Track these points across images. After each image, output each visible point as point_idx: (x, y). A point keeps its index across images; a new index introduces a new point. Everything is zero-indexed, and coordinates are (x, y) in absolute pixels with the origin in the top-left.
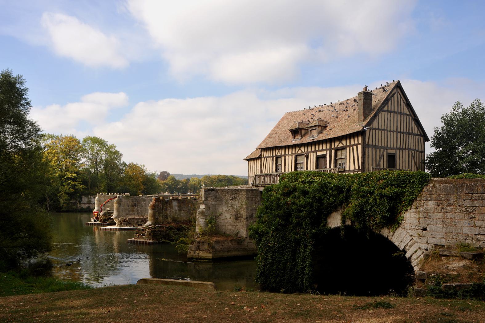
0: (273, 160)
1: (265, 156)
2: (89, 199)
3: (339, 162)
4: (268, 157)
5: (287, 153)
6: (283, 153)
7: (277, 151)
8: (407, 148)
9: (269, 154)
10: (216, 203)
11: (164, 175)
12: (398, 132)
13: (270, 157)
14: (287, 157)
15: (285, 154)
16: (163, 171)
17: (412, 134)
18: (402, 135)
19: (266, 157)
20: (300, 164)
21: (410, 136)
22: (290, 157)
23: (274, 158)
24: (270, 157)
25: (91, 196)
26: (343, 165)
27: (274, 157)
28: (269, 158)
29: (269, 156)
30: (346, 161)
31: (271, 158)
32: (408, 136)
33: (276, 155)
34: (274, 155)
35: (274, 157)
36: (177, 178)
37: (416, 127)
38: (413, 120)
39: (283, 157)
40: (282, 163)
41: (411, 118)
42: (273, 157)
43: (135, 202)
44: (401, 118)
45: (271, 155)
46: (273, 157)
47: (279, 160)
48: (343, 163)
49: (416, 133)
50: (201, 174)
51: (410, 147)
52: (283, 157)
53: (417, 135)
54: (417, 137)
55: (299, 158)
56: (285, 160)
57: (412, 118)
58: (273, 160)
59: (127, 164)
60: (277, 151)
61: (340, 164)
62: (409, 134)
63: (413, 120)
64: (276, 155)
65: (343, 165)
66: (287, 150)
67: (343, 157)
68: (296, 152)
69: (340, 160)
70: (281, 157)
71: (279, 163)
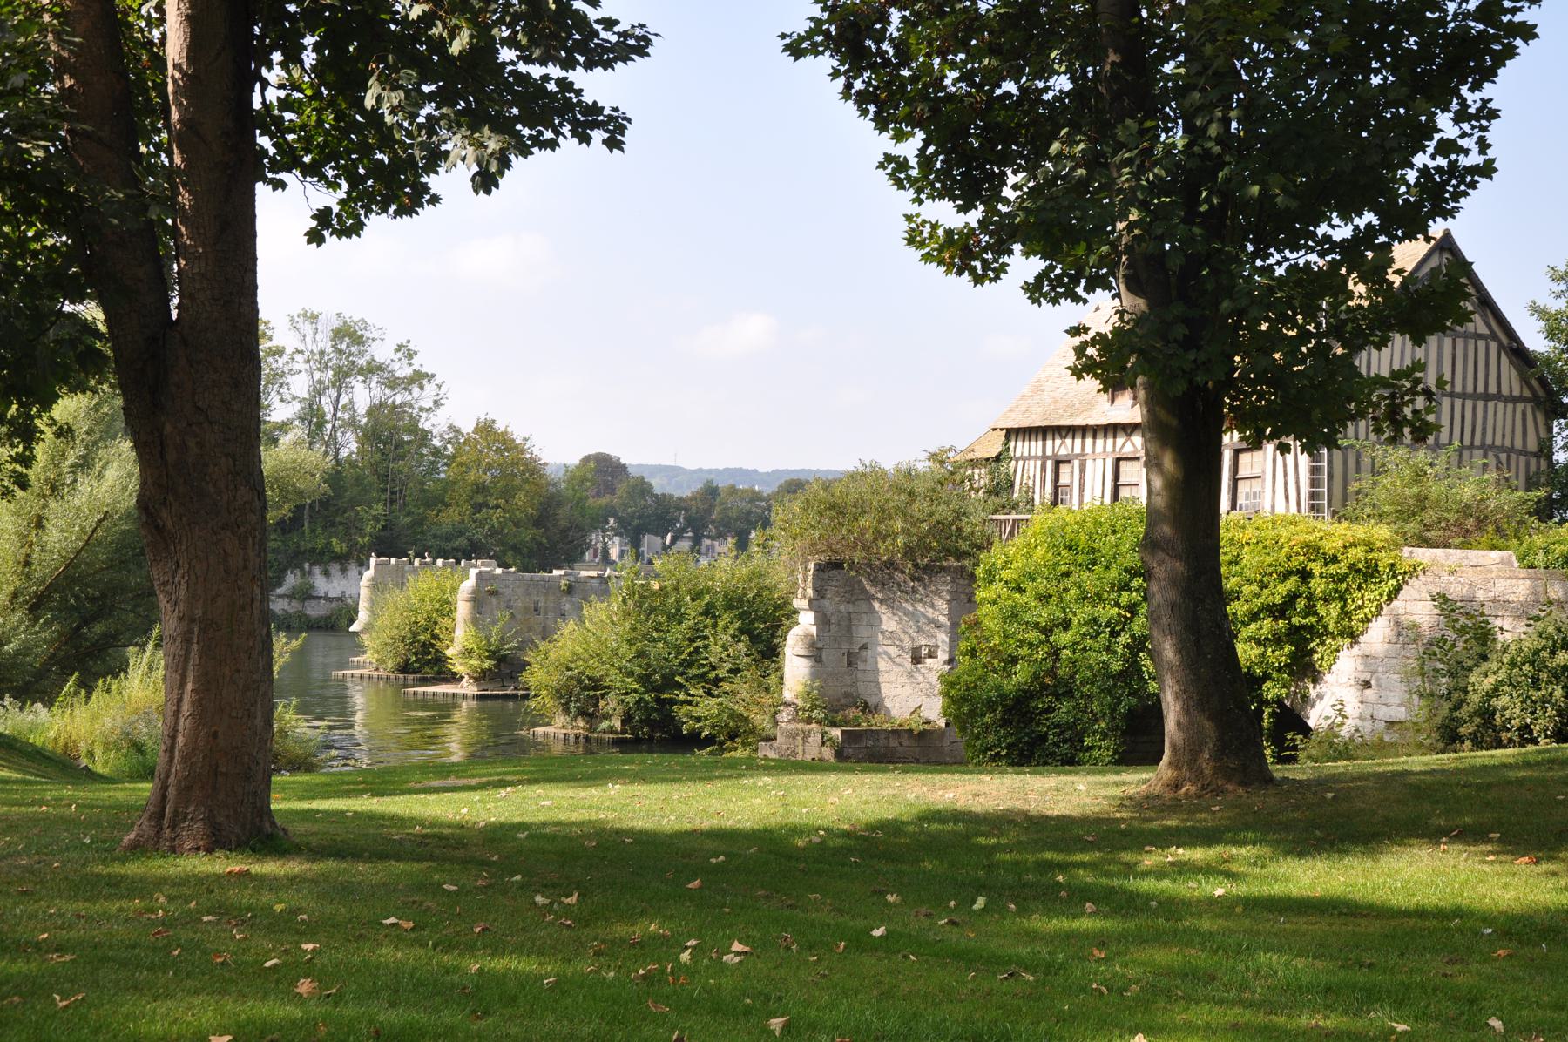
0: (1043, 469)
1: (1018, 454)
2: (303, 576)
3: (1243, 488)
4: (1030, 458)
5: (1088, 449)
6: (1078, 450)
7: (1058, 442)
8: (1477, 442)
9: (1034, 447)
10: (851, 608)
11: (604, 469)
12: (1459, 396)
13: (1036, 458)
14: (1089, 464)
15: (1083, 454)
16: (593, 452)
17: (1498, 396)
18: (1458, 402)
19: (1022, 458)
20: (1128, 488)
21: (1491, 404)
22: (1100, 462)
23: (1049, 464)
24: (1036, 458)
25: (311, 565)
26: (1255, 498)
27: (1048, 458)
28: (1032, 462)
29: (1033, 454)
30: (1263, 487)
31: (1039, 463)
32: (1480, 404)
33: (1055, 455)
34: (1049, 452)
35: (1048, 458)
36: (659, 485)
37: (1514, 373)
38: (1503, 354)
39: (1076, 463)
40: (1072, 482)
41: (1493, 345)
42: (1044, 458)
43: (536, 598)
44: (1454, 348)
45: (1040, 453)
46: (1044, 458)
47: (1064, 469)
48: (1255, 493)
49: (1516, 392)
50: (764, 467)
51: (1489, 441)
52: (1076, 463)
53: (1521, 399)
54: (1520, 407)
55: (1124, 466)
56: (1083, 470)
57: (1501, 347)
58: (1043, 469)
59: (464, 432)
60: (1058, 442)
61: (1247, 494)
62: (1487, 397)
63: (1503, 354)
64: (1055, 455)
65: (1255, 498)
66: (1089, 441)
67: (1256, 472)
68: (1117, 449)
69: (1248, 482)
70: (1069, 461)
71: (1064, 480)
